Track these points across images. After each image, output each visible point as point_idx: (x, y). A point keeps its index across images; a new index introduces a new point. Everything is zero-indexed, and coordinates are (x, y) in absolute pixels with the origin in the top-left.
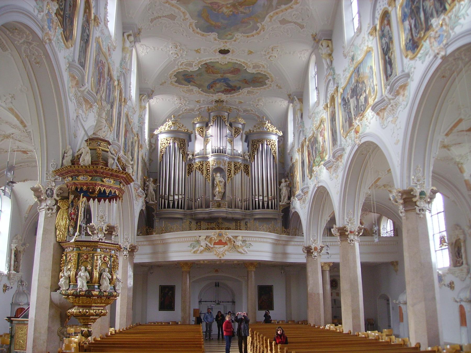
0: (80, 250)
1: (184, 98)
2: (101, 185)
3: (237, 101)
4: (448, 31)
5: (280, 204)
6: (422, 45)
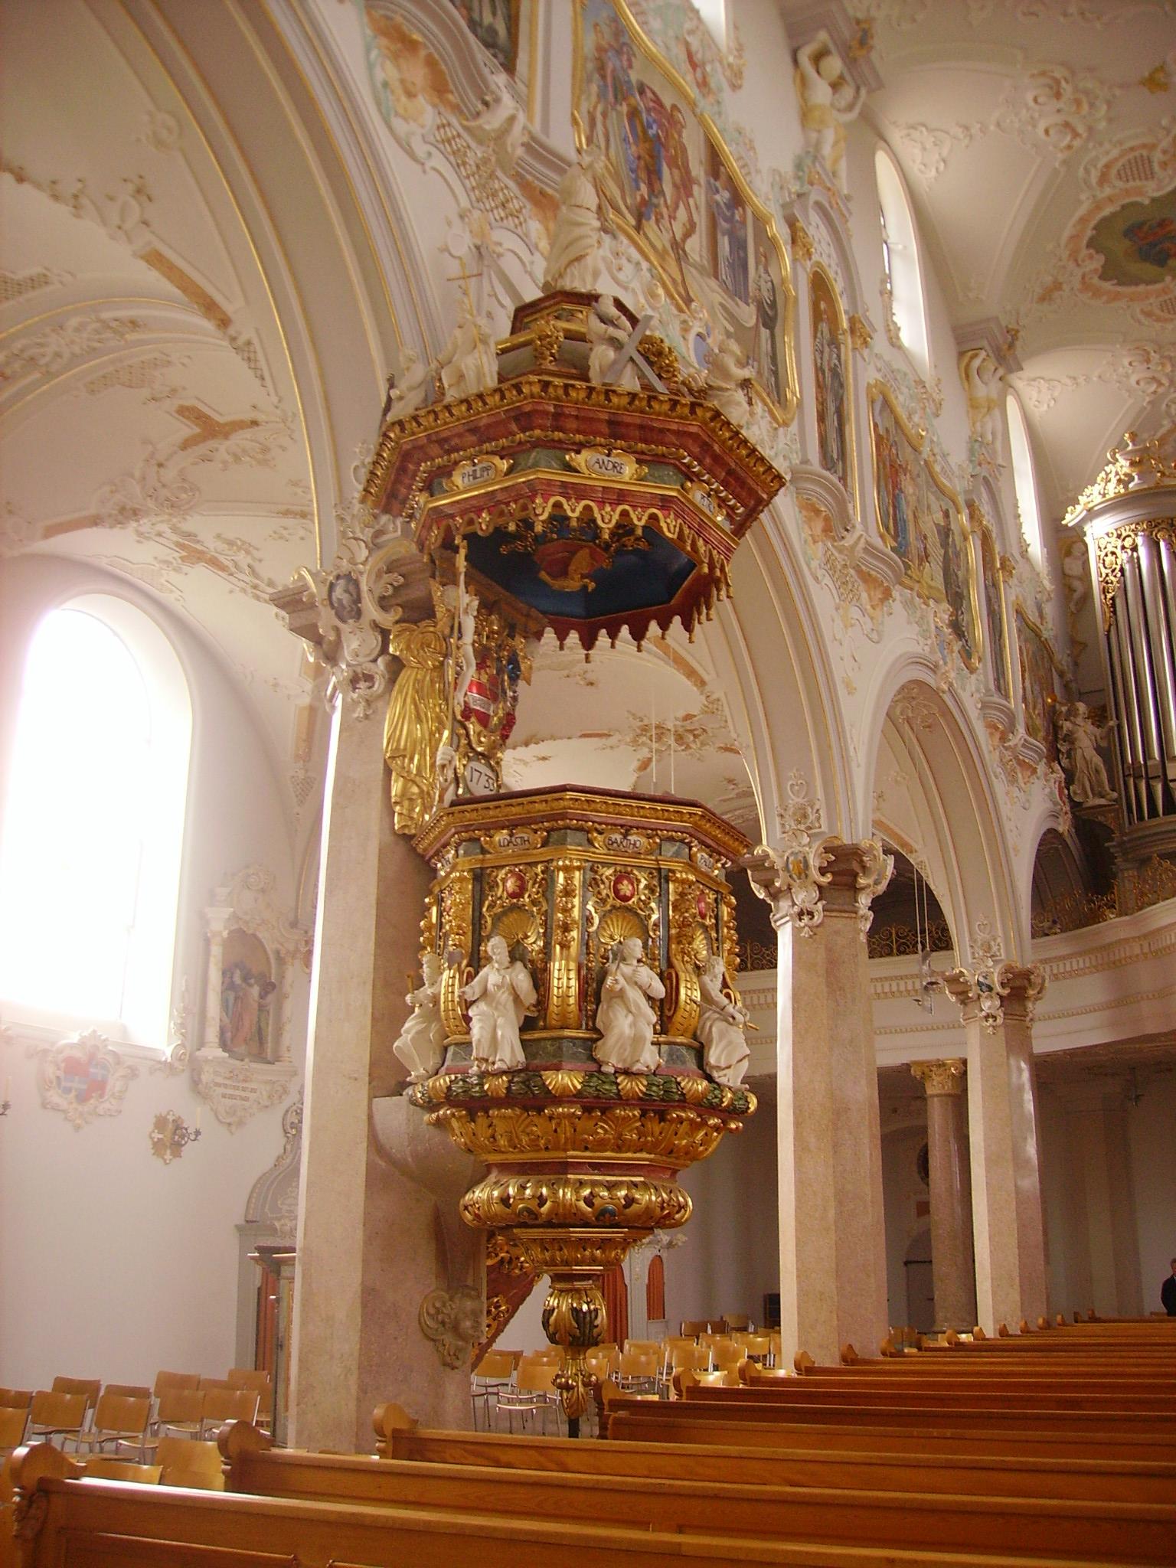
0: (484, 851)
1: (1159, 348)
2: (566, 489)
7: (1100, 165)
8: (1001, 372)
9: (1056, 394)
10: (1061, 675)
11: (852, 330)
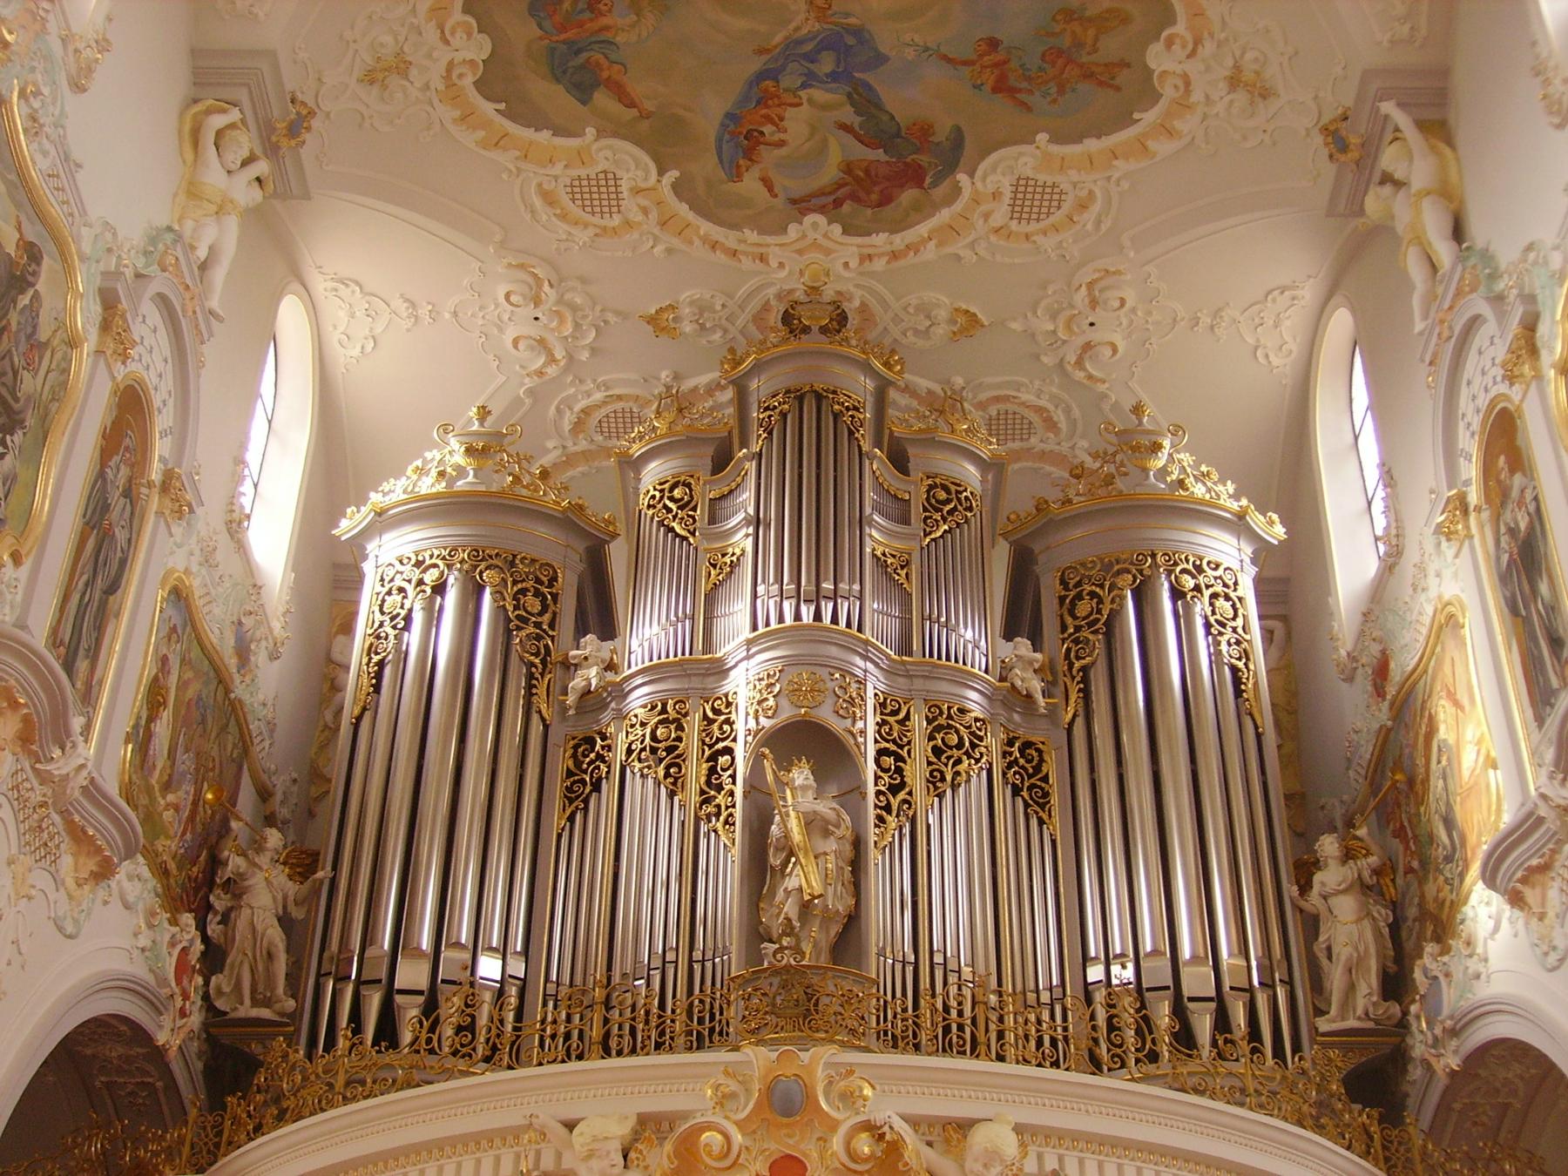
3: (944, 303)
5: (1324, 1025)
7: (577, 408)
8: (262, 167)
9: (378, 330)
10: (264, 794)
11: (165, 488)
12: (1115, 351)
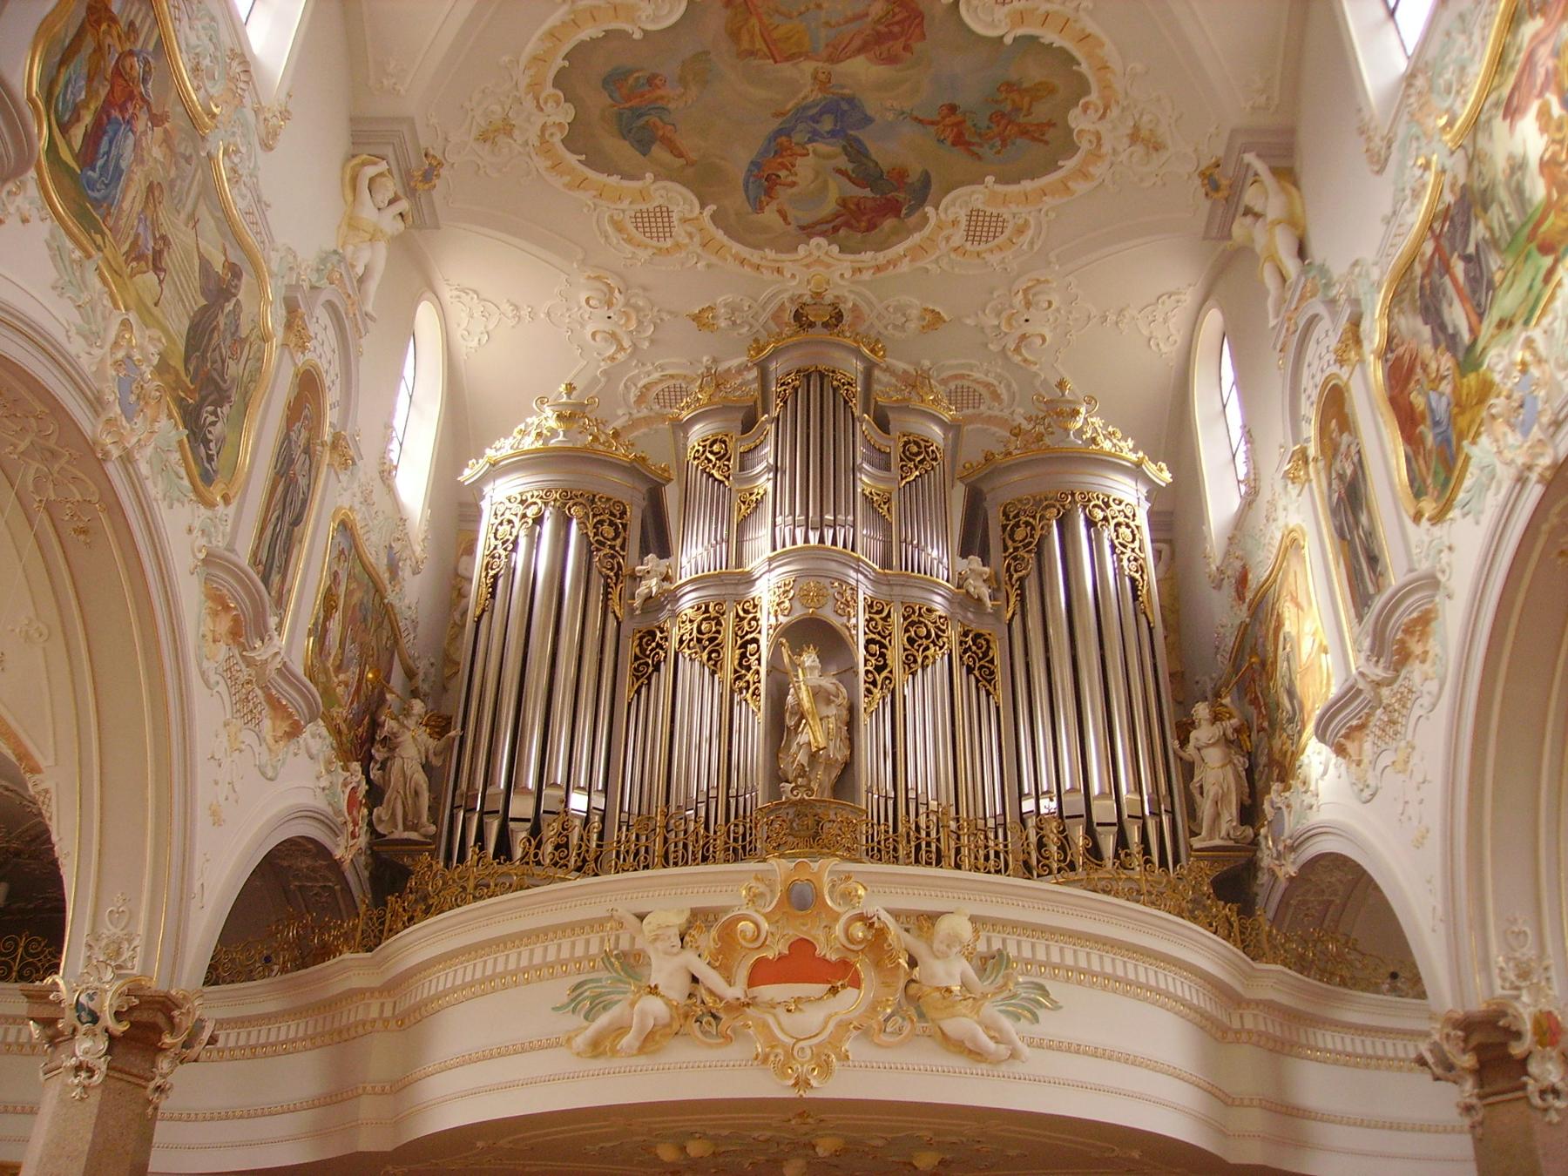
4: (1552, 377)
5: (1197, 843)
6: (1468, 458)
7: (640, 385)
9: (491, 327)
10: (410, 674)
11: (334, 446)
12: (1044, 340)
